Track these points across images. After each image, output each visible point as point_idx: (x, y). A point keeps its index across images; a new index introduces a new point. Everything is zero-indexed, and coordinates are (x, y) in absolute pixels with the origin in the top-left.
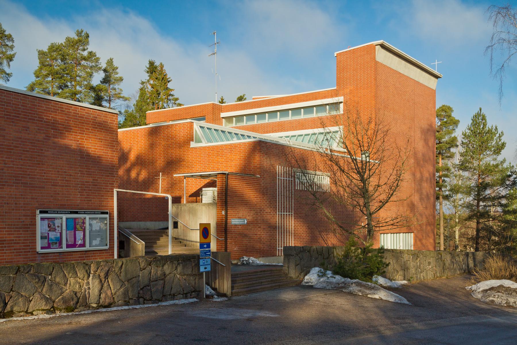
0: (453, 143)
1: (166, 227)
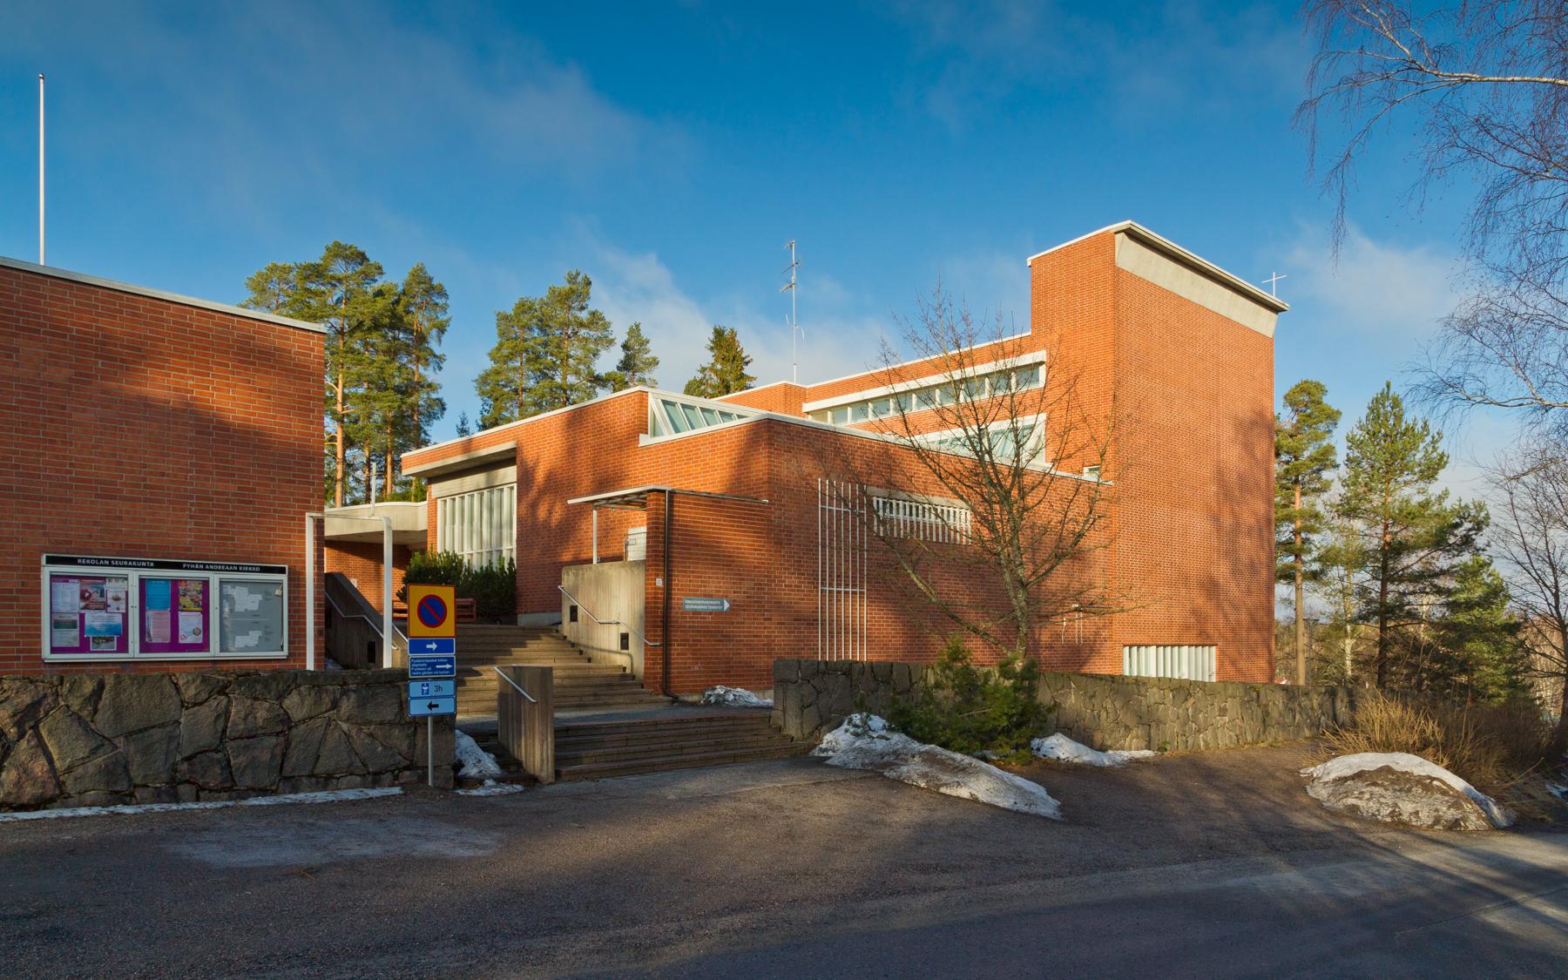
0: (1324, 460)
1: (556, 621)
